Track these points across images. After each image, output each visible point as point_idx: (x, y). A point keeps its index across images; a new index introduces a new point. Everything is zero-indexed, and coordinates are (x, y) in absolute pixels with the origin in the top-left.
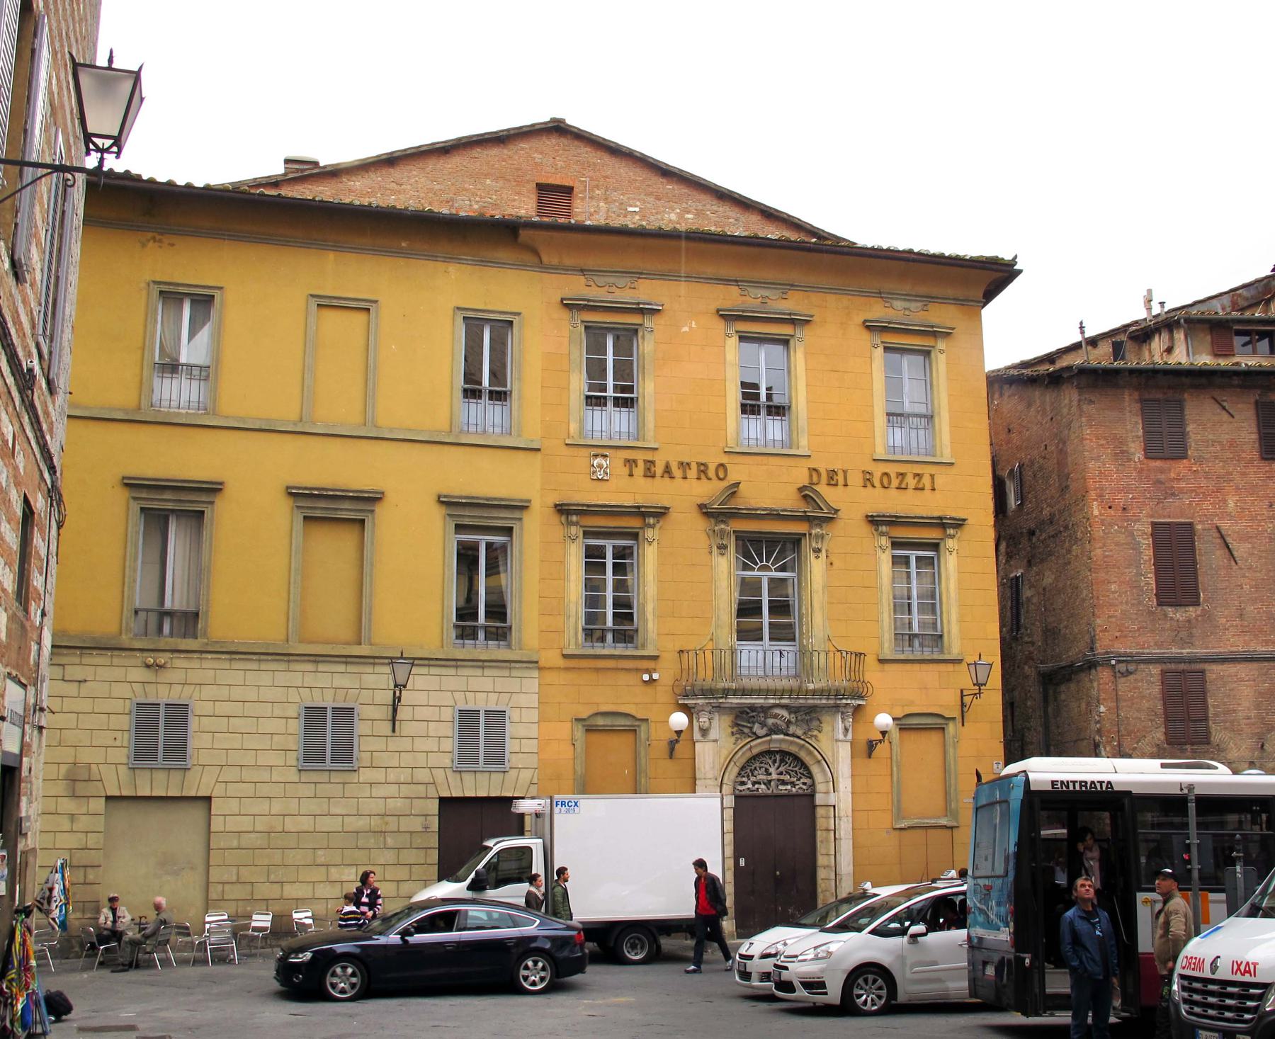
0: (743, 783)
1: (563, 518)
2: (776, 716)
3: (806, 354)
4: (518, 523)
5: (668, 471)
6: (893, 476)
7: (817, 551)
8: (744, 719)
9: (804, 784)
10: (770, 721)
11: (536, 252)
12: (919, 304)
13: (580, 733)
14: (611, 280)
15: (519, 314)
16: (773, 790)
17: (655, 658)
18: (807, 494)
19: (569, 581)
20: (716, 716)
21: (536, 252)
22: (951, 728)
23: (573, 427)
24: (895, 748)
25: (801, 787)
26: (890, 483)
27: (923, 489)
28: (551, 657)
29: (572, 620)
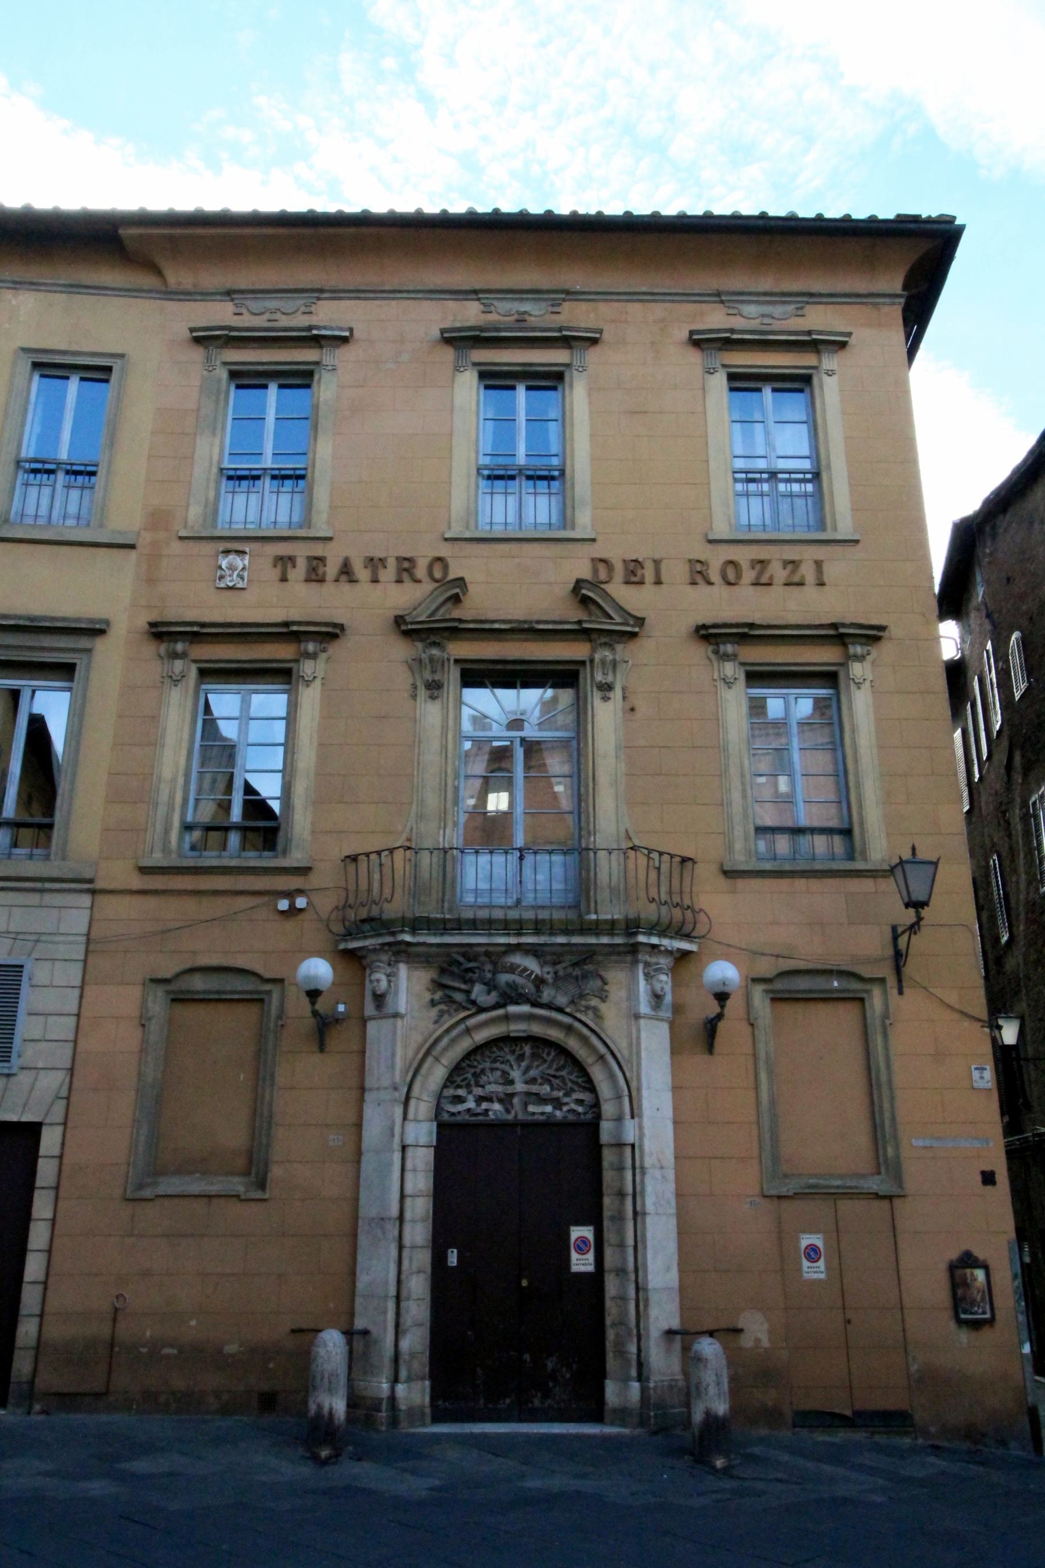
0: (459, 1100)
1: (163, 648)
2: (512, 969)
3: (590, 391)
4: (84, 656)
5: (346, 571)
6: (745, 566)
7: (606, 688)
8: (457, 973)
9: (580, 1102)
10: (504, 978)
11: (158, 272)
12: (790, 308)
13: (158, 1004)
14: (272, 304)
15: (122, 356)
16: (517, 1112)
17: (304, 871)
18: (582, 594)
19: (163, 746)
20: (403, 969)
21: (158, 272)
22: (876, 1000)
23: (195, 512)
24: (761, 1037)
25: (573, 1105)
26: (739, 575)
27: (801, 584)
28: (119, 873)
29: (162, 810)
